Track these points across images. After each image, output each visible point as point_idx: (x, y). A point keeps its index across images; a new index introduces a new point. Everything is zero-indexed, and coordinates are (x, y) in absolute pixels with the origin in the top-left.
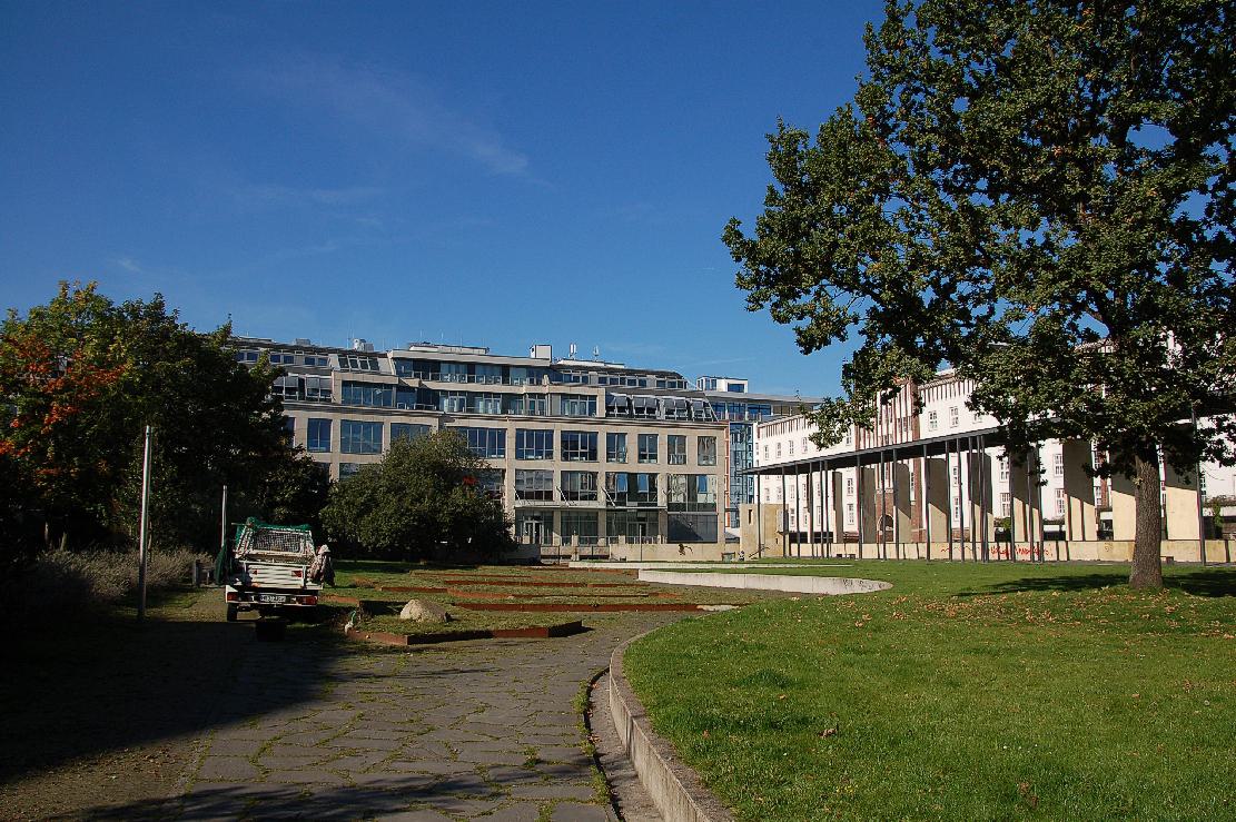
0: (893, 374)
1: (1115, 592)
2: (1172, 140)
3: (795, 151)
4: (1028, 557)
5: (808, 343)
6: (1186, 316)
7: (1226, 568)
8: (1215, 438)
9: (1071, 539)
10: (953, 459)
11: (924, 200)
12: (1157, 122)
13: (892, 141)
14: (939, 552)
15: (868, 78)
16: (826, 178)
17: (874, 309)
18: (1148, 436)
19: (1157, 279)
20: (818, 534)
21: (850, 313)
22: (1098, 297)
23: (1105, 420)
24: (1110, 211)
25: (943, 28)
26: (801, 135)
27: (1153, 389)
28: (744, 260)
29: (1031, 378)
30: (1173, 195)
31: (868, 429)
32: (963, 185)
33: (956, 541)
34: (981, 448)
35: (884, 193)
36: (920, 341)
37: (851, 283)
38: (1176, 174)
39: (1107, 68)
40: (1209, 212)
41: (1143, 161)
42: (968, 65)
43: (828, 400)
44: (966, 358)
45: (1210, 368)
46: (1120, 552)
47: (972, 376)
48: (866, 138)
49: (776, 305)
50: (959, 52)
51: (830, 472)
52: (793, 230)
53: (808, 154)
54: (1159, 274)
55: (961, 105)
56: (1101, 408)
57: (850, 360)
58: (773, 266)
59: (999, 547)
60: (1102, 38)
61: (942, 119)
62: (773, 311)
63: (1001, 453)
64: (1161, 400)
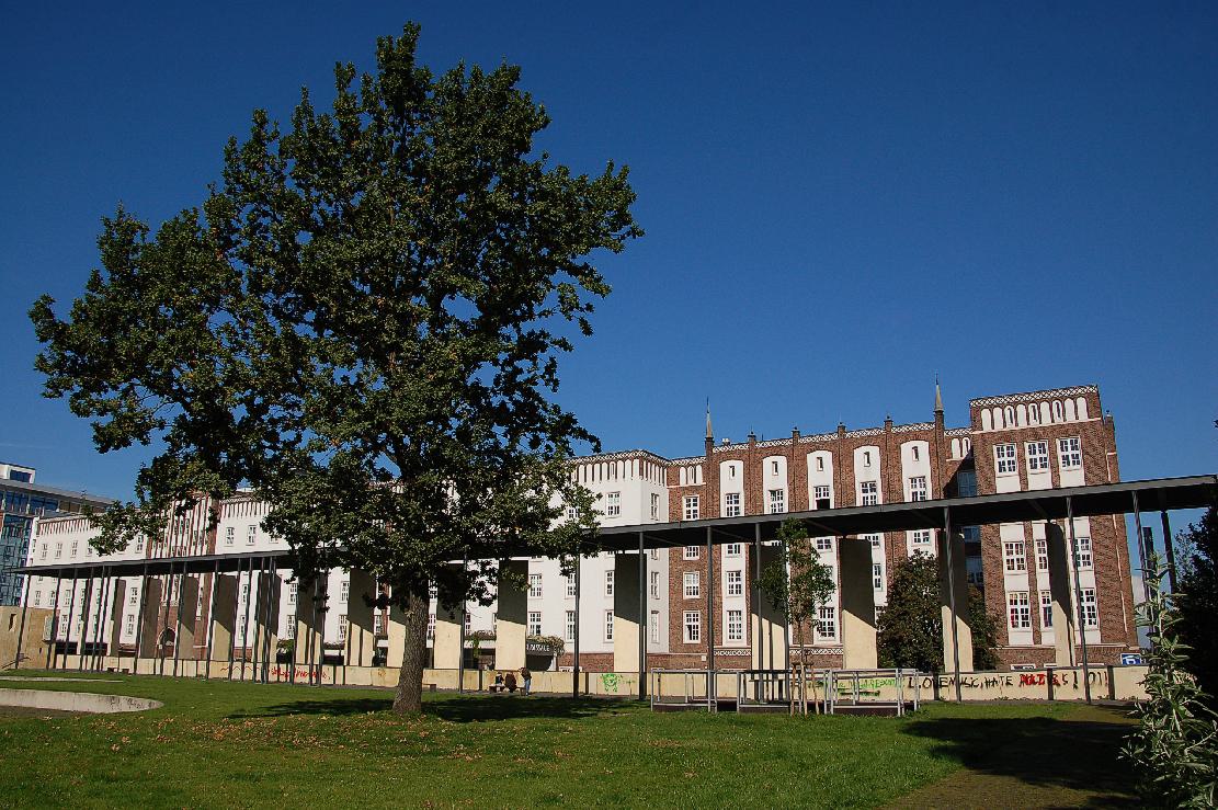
0: (190, 485)
1: (378, 718)
2: (478, 314)
3: (131, 242)
4: (307, 680)
5: (106, 441)
6: (467, 470)
7: (477, 695)
8: (479, 579)
9: (348, 664)
10: (244, 577)
11: (253, 320)
12: (467, 296)
13: (232, 255)
14: (218, 671)
15: (221, 188)
16: (157, 277)
17: (183, 417)
18: (423, 573)
19: (448, 432)
20: (89, 645)
21: (156, 417)
22: (397, 441)
23: (388, 554)
24: (418, 364)
25: (301, 162)
26: (140, 227)
27: (432, 530)
28: (50, 342)
29: (326, 507)
30: (472, 362)
31: (157, 539)
32: (293, 313)
33: (570, 654)
34: (272, 569)
35: (215, 303)
36: (224, 458)
37: (162, 387)
38: (475, 345)
39: (436, 238)
40: (497, 382)
41: (451, 327)
42: (318, 203)
43: (117, 504)
44: (266, 481)
45: (480, 518)
46: (390, 679)
47: (268, 499)
48: (207, 247)
49: (77, 396)
50: (312, 189)
51: (113, 579)
52: (110, 322)
53: (144, 247)
54: (451, 428)
55: (304, 238)
56: (385, 543)
57: (149, 465)
58: (82, 354)
59: (279, 669)
60: (436, 213)
61: (284, 247)
62: (72, 402)
63: (289, 577)
64: (436, 541)
